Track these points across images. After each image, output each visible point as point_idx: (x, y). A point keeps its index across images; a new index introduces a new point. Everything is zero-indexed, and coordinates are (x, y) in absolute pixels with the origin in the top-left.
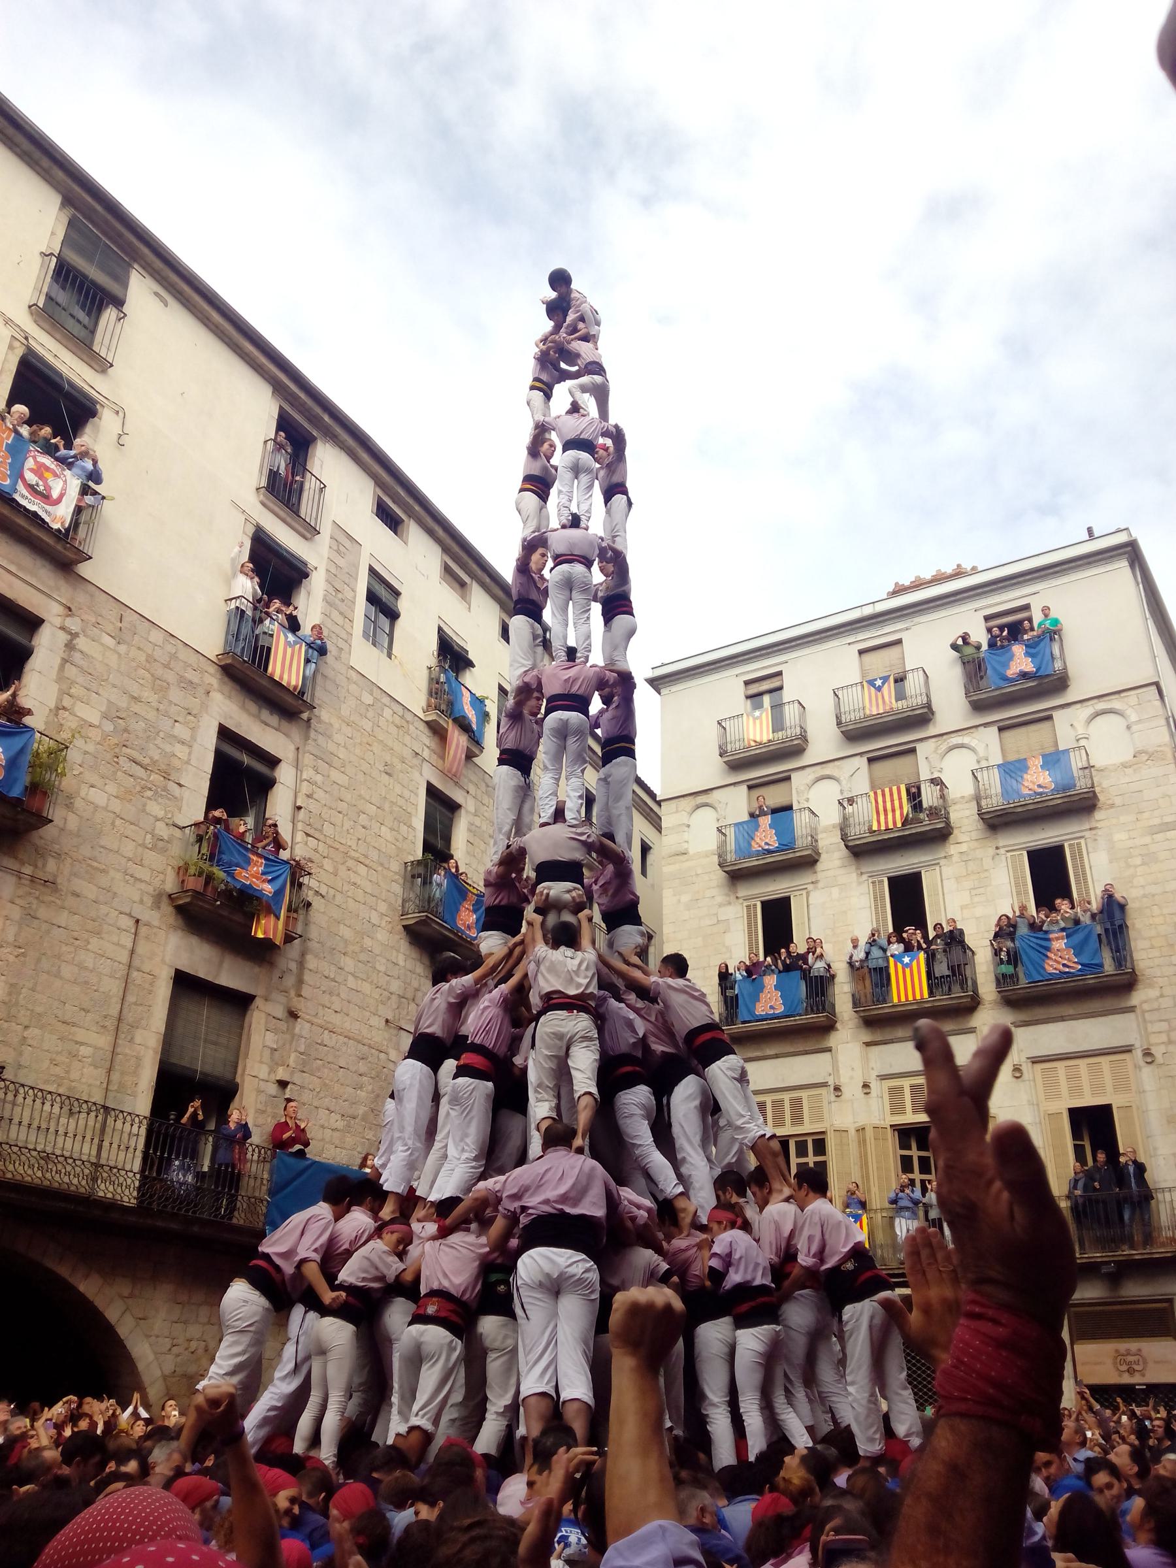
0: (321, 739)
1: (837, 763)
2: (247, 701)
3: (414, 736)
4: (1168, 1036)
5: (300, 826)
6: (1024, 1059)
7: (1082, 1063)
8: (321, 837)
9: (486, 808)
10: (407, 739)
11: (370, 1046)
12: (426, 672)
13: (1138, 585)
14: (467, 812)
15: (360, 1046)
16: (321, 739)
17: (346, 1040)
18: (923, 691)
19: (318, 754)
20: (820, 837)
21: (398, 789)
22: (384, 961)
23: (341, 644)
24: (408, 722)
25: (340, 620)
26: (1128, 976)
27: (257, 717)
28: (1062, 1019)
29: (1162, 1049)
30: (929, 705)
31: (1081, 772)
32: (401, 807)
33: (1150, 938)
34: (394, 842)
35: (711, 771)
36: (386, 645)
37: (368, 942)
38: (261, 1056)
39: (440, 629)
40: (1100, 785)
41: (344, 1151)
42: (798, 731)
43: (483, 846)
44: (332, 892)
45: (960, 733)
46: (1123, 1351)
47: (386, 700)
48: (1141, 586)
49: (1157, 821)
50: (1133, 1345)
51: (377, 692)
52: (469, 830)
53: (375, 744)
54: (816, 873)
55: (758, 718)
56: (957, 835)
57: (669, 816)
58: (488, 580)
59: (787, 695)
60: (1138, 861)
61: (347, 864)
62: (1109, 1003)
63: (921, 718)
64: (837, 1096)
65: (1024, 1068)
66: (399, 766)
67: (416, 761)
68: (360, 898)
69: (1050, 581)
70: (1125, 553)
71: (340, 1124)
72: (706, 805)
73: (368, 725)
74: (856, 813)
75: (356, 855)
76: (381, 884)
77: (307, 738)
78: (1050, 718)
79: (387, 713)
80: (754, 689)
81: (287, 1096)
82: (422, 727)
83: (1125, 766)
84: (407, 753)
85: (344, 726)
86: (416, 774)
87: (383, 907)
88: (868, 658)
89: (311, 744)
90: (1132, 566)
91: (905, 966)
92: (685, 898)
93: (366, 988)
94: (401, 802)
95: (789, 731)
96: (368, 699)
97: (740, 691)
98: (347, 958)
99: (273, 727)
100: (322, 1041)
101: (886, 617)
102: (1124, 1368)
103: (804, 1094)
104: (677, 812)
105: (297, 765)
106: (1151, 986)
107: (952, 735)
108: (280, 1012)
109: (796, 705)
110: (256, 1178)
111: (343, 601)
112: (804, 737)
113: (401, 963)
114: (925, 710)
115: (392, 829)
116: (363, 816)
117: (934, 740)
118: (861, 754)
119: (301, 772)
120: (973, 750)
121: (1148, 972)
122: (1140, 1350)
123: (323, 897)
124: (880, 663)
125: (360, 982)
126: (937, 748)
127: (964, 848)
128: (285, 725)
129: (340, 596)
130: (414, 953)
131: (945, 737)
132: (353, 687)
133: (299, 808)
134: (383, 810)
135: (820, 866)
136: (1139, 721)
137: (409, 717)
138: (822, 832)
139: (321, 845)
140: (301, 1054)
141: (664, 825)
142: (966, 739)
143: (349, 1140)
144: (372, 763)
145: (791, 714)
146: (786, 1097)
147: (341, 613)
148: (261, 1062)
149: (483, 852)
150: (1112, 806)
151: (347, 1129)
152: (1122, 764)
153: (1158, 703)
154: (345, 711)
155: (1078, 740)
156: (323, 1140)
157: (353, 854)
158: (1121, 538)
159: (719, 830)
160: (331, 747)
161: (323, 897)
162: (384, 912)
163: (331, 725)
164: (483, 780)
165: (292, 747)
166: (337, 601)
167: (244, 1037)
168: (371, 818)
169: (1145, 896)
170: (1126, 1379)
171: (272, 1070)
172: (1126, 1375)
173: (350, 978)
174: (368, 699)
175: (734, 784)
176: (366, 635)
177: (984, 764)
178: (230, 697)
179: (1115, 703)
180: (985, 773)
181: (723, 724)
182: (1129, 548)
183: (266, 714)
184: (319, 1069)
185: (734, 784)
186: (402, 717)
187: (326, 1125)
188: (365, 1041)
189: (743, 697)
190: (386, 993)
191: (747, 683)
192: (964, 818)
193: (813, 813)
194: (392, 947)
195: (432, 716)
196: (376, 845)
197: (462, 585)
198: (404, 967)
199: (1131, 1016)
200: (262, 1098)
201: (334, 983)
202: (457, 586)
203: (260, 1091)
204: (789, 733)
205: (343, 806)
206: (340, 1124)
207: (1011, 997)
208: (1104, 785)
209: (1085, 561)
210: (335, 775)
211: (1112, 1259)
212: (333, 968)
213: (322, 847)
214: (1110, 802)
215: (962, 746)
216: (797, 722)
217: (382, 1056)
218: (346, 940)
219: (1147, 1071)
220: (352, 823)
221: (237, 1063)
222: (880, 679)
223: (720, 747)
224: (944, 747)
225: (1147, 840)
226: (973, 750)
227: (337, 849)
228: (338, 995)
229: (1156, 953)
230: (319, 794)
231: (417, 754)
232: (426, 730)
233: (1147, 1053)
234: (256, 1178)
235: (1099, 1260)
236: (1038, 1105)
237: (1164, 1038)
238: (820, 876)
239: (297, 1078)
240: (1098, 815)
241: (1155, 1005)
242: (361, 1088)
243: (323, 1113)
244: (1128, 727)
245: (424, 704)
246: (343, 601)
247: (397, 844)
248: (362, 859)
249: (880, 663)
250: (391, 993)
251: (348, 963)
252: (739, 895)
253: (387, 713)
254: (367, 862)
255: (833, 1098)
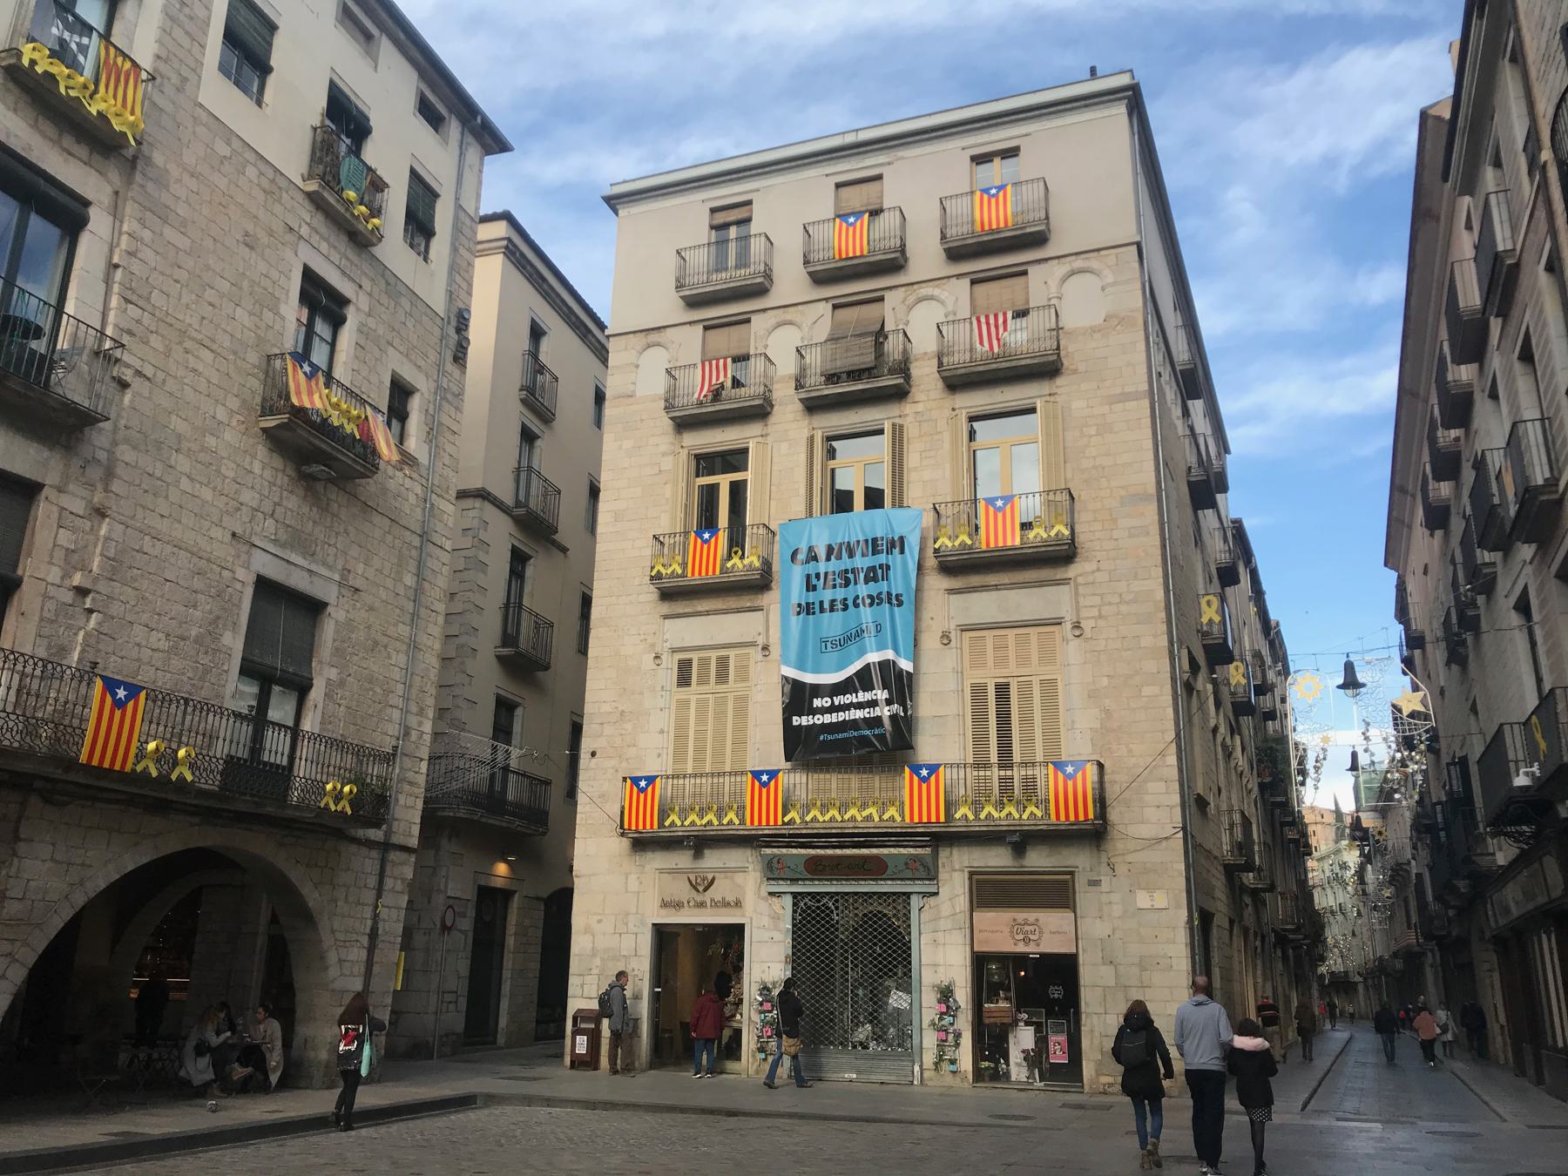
0: (150, 186)
1: (800, 307)
2: (40, 119)
3: (288, 207)
4: (1099, 610)
5: (116, 288)
6: (953, 627)
7: (1011, 633)
8: (149, 308)
9: (383, 309)
10: (278, 209)
11: (209, 560)
12: (309, 135)
13: (1134, 134)
14: (358, 309)
15: (197, 560)
16: (150, 186)
17: (175, 549)
18: (898, 233)
19: (147, 204)
20: (776, 386)
21: (262, 267)
22: (234, 466)
23: (185, 72)
24: (280, 188)
25: (186, 42)
26: (1066, 547)
27: (57, 143)
28: (996, 587)
29: (1092, 623)
30: (902, 249)
31: (1048, 334)
32: (265, 289)
33: (1094, 511)
34: (253, 328)
35: (668, 307)
36: (255, 90)
37: (211, 441)
38: (52, 557)
39: (332, 83)
40: (1066, 348)
41: (169, 675)
42: (762, 268)
43: (376, 351)
44: (161, 375)
45: (931, 284)
46: (1020, 921)
47: (249, 156)
48: (1136, 137)
49: (1118, 391)
50: (1031, 915)
51: (236, 144)
52: (359, 331)
53: (232, 206)
54: (766, 425)
55: (994, 195)
56: (917, 393)
57: (618, 353)
58: (402, 36)
59: (755, 228)
60: (1093, 431)
61: (185, 345)
62: (746, 601)
63: (893, 264)
64: (765, 656)
65: (952, 636)
66: (265, 240)
67: (290, 237)
68: (203, 386)
69: (1044, 123)
70: (1124, 98)
71: (164, 645)
72: (658, 345)
73: (222, 183)
74: (813, 365)
75: (200, 337)
76: (233, 375)
77: (129, 181)
78: (1025, 273)
79: (251, 172)
80: (721, 218)
81: (87, 606)
82: (300, 197)
83: (1094, 330)
84: (279, 227)
85: (186, 177)
86: (288, 253)
87: (234, 403)
88: (846, 192)
89: (134, 191)
90: (1130, 115)
91: (997, 510)
92: (627, 444)
93: (207, 494)
94: (266, 283)
95: (752, 266)
96: (223, 150)
97: (704, 219)
98: (180, 456)
99: (80, 159)
100: (142, 547)
101: (869, 148)
102: (1021, 937)
103: (732, 653)
104: (626, 349)
105: (116, 212)
106: (1087, 559)
107: (923, 285)
108: (78, 506)
109: (763, 238)
110: (38, 696)
111: (191, 18)
112: (768, 275)
113: (257, 470)
114: (898, 255)
115: (251, 314)
116: (209, 292)
117: (903, 289)
118: (826, 299)
119: (122, 222)
120: (942, 303)
121: (1087, 545)
122: (1037, 920)
123: (148, 379)
124: (857, 198)
125: (198, 486)
126: (905, 299)
127: (920, 407)
128: (96, 157)
129: (187, 10)
130: (278, 462)
131: (915, 287)
132: (200, 130)
133: (116, 266)
134: (241, 288)
135: (772, 419)
136: (1114, 284)
137: (282, 183)
138: (778, 382)
139: (146, 317)
140: (109, 558)
141: (610, 363)
142: (936, 292)
143: (175, 663)
144: (227, 229)
145: (757, 247)
146: (714, 655)
147: (187, 33)
148: (51, 563)
149: (376, 359)
150: (1075, 372)
151: (175, 650)
152: (1091, 328)
153: (1136, 265)
154: (189, 158)
155: (1050, 299)
156: (138, 660)
157: (195, 334)
158: (1124, 80)
159: (668, 372)
160: (165, 198)
161: (148, 379)
162: (235, 409)
163: (167, 171)
164: (383, 276)
165: (109, 190)
166: (182, 17)
167: (28, 532)
168: (222, 296)
169: (1095, 467)
170: (1021, 948)
171: (66, 575)
172: (1021, 944)
173: (184, 480)
174: (223, 150)
175: (690, 323)
176: (223, 69)
177: (951, 318)
178: (15, 110)
179: (1094, 262)
180: (951, 327)
181: (683, 254)
182: (1131, 93)
183: (68, 141)
184: (134, 579)
185: (690, 323)
186: (273, 181)
187: (144, 643)
188: (202, 554)
189: (707, 227)
190: (232, 503)
191: (713, 211)
192: (925, 375)
193: (770, 360)
194: (246, 452)
195: (312, 186)
196: (229, 329)
197: (368, 37)
198: (261, 476)
199: (1066, 588)
200: (51, 605)
201: (159, 483)
202: (362, 39)
203: (46, 597)
204: (752, 270)
205: (182, 275)
206: (164, 645)
207: (947, 564)
208: (1070, 350)
209: (1083, 103)
210: (169, 232)
211: (1018, 828)
212: (159, 465)
213: (147, 319)
214: (1073, 367)
215: (931, 298)
216: (762, 258)
217: (226, 574)
218: (180, 435)
219: (1074, 643)
220: (194, 297)
221: (18, 561)
222: (996, 188)
223: (678, 280)
224: (912, 299)
225: (1106, 409)
226: (942, 303)
227: (171, 325)
228: (167, 497)
229: (1098, 526)
230: (147, 254)
231: (291, 229)
232: (307, 203)
233: (1077, 626)
234: (38, 696)
235: (1004, 828)
236: (962, 672)
237: (1095, 612)
238: (770, 429)
239: (102, 587)
240: (1060, 381)
241: (1090, 579)
242: (195, 607)
243: (138, 630)
244: (1103, 289)
245: (304, 170)
246: (191, 18)
247: (259, 332)
248: (209, 344)
249: (857, 198)
250: (241, 504)
251: (183, 463)
252: (684, 444)
253: (251, 172)
254: (214, 347)
255: (760, 657)
